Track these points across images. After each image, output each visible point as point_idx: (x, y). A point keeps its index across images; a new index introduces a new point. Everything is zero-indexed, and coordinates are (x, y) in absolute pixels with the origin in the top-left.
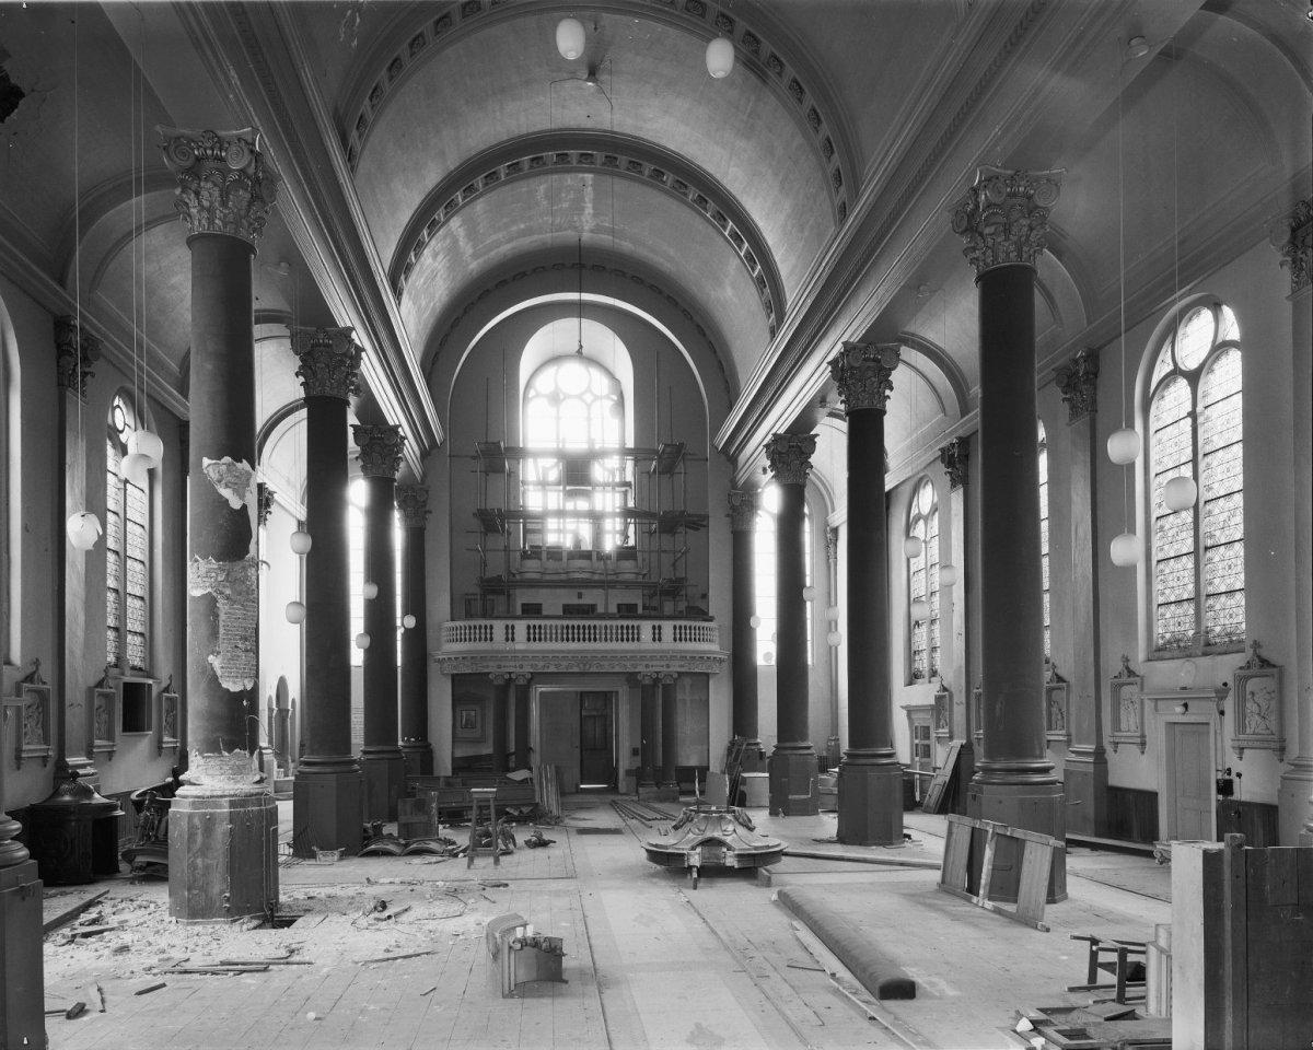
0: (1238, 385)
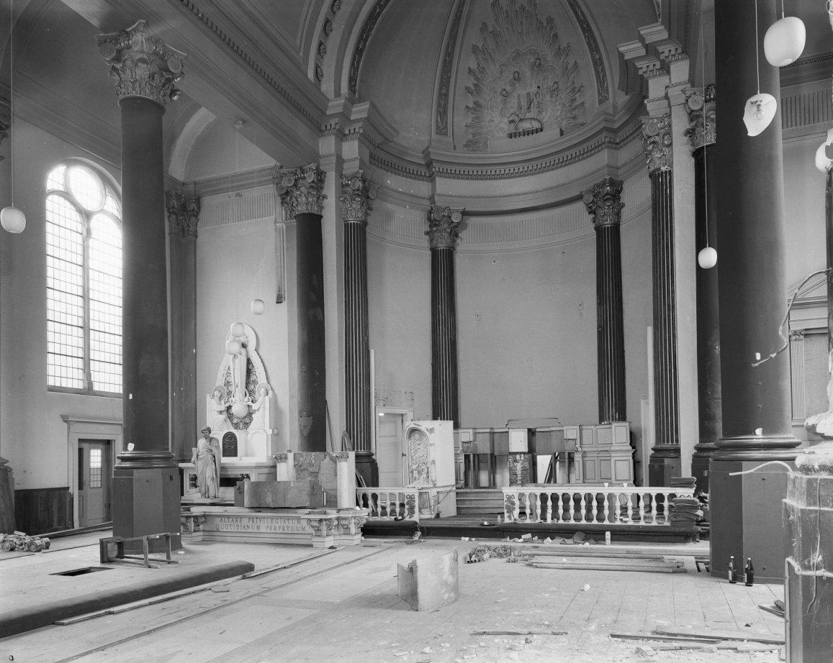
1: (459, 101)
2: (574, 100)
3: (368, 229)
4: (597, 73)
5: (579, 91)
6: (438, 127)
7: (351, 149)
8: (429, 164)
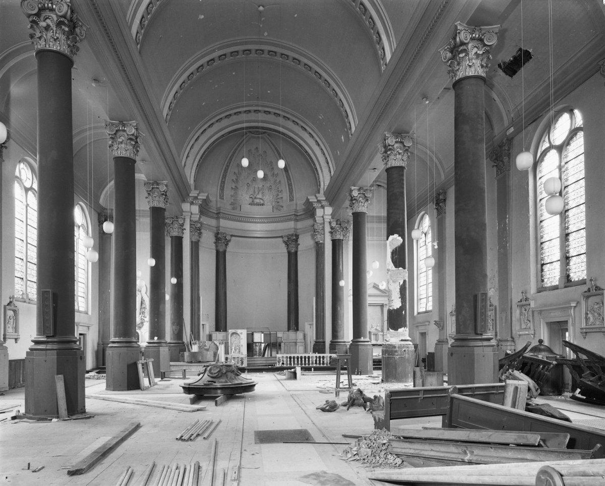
0: (582, 150)
1: (229, 185)
2: (278, 195)
3: (200, 244)
6: (220, 195)
7: (195, 209)
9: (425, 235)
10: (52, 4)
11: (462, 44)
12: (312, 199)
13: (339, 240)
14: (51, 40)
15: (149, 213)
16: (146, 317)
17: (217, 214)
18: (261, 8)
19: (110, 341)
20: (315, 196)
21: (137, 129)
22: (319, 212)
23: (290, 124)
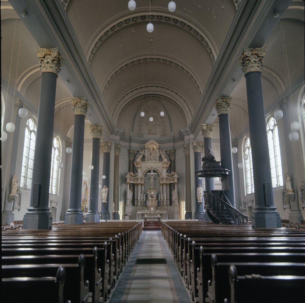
4: (170, 125)
5: (165, 127)
6: (132, 130)
7: (118, 138)
8: (130, 139)
9: (248, 149)
10: (50, 52)
11: (247, 57)
12: (183, 130)
13: (198, 153)
14: (49, 68)
15: (92, 141)
16: (88, 198)
17: (130, 139)
18: (152, 40)
19: (67, 210)
20: (184, 129)
21: (87, 101)
22: (186, 137)
23: (169, 92)
